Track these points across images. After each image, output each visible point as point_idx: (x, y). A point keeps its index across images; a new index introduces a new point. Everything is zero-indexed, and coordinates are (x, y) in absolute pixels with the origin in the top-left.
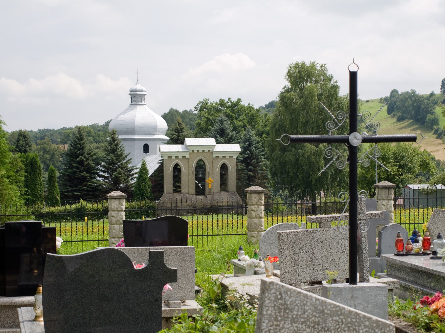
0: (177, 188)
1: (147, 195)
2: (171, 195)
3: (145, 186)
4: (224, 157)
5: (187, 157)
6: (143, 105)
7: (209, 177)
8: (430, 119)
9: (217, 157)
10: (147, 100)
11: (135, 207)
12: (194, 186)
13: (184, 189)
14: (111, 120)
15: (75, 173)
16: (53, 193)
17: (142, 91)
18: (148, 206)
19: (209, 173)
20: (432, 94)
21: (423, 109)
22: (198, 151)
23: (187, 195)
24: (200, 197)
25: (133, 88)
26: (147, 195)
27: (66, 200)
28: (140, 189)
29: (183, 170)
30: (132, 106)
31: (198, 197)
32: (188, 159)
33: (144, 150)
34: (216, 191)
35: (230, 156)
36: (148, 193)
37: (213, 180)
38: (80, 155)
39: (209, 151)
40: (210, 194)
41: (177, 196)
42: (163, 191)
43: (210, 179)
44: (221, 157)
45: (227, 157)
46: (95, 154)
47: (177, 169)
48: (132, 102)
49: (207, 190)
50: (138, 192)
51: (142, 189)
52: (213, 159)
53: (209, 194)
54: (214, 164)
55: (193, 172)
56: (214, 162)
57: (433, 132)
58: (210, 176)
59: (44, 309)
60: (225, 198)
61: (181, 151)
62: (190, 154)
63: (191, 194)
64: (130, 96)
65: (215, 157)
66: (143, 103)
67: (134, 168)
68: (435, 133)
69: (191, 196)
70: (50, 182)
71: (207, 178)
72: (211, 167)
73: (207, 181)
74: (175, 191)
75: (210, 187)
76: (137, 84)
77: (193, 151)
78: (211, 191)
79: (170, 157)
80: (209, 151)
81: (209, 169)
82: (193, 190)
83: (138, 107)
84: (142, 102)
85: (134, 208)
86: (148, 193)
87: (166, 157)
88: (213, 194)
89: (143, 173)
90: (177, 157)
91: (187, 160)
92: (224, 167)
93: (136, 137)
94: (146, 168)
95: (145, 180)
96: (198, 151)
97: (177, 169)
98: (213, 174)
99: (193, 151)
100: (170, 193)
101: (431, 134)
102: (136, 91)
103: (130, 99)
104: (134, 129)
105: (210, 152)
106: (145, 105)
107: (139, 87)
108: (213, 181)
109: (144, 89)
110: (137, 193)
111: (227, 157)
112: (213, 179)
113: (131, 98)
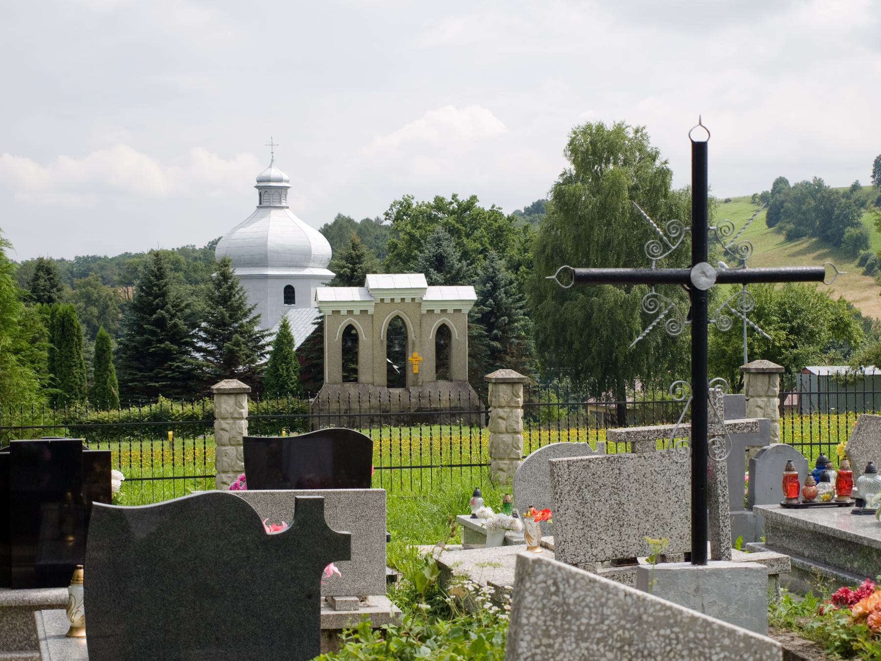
0: (350, 373)
1: (292, 386)
2: (339, 386)
3: (287, 369)
4: (444, 311)
5: (371, 311)
6: (282, 208)
7: (413, 351)
8: (851, 236)
9: (431, 312)
10: (290, 199)
11: (266, 411)
12: (384, 370)
13: (364, 376)
14: (220, 238)
15: (148, 343)
16: (105, 383)
17: (281, 181)
18: (293, 408)
19: (414, 344)
20: (855, 187)
21: (838, 217)
22: (392, 300)
23: (370, 386)
24: (396, 391)
25: (263, 175)
26: (292, 386)
27: (130, 396)
28: (277, 376)
29: (363, 338)
30: (261, 210)
31: (391, 390)
32: (372, 316)
33: (285, 298)
34: (428, 379)
35: (454, 310)
36: (293, 384)
37: (421, 358)
38: (158, 307)
39: (413, 299)
40: (415, 384)
41: (351, 389)
42: (322, 379)
43: (415, 355)
44: (437, 311)
45: (450, 311)
46: (188, 306)
47: (350, 336)
48: (260, 203)
49: (410, 378)
50: (273, 381)
51: (281, 376)
52: (422, 315)
53: (414, 386)
54: (424, 325)
55: (382, 342)
56: (424, 321)
57: (857, 261)
58: (417, 349)
59: (86, 613)
60: (445, 394)
61: (359, 299)
62: (375, 307)
63: (379, 386)
64: (257, 191)
65: (425, 312)
66: (284, 204)
67: (266, 333)
68: (861, 265)
69: (379, 389)
70: (100, 362)
71: (410, 354)
72: (418, 331)
73: (410, 358)
74: (346, 379)
75: (416, 371)
76: (270, 167)
77: (382, 300)
78: (417, 379)
79: (336, 312)
80: (413, 299)
81: (413, 335)
82: (381, 377)
83: (274, 212)
84: (280, 202)
85: (265, 413)
86: (293, 384)
87: (328, 311)
88: (422, 386)
89: (283, 343)
90: (350, 312)
91: (370, 318)
92: (443, 332)
93: (270, 272)
94: (289, 334)
95: (286, 358)
96: (392, 300)
97: (350, 336)
98: (421, 345)
99: (382, 300)
100: (336, 383)
101: (852, 265)
102: (269, 181)
103: (258, 197)
104: (266, 256)
105: (416, 301)
106: (287, 207)
107: (274, 173)
108: (421, 358)
109: (285, 177)
110: (271, 382)
111: (450, 311)
112: (423, 356)
113: (260, 195)
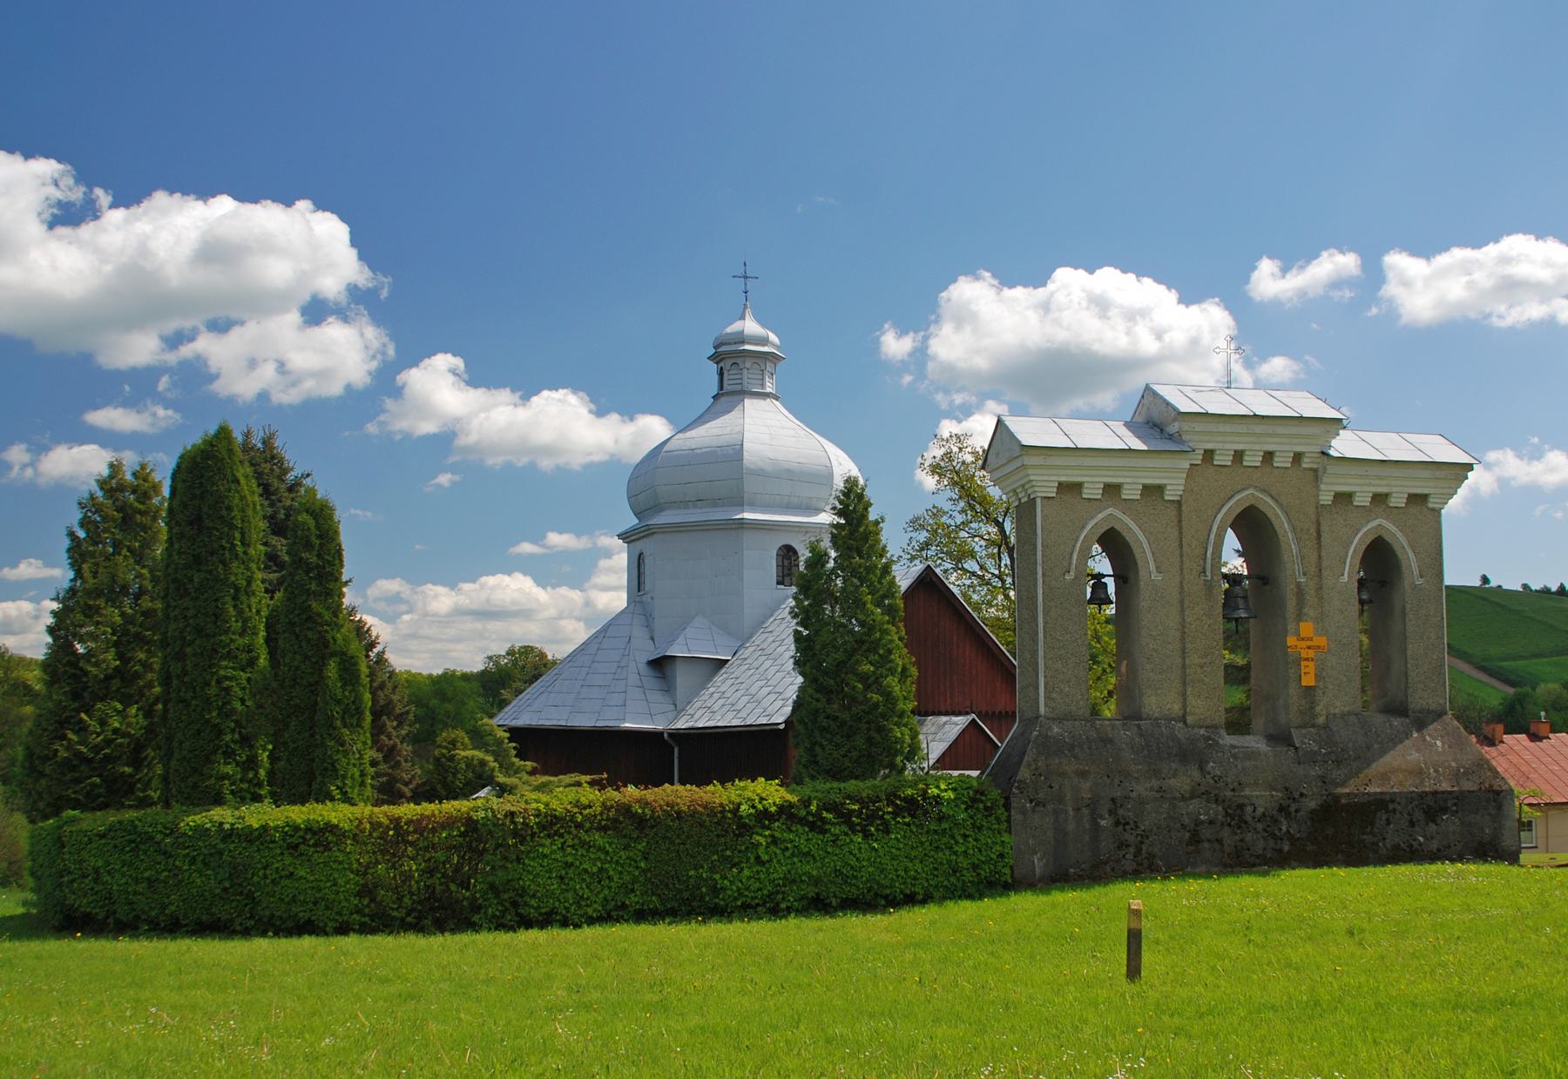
4: (1112, 490)
5: (1175, 488)
7: (1300, 617)
9: (1344, 498)
19: (1300, 592)
22: (1239, 456)
30: (723, 399)
35: (1146, 488)
43: (1306, 628)
44: (1093, 491)
45: (1398, 500)
52: (1320, 508)
54: (1326, 538)
58: (1310, 611)
59: (443, 585)
65: (1326, 498)
71: (1291, 627)
73: (1291, 640)
75: (1308, 681)
77: (1209, 454)
79: (1070, 489)
80: (1298, 457)
84: (763, 385)
87: (1045, 484)
91: (1172, 512)
103: (716, 378)
108: (1321, 641)
111: (1131, 493)
113: (721, 374)
